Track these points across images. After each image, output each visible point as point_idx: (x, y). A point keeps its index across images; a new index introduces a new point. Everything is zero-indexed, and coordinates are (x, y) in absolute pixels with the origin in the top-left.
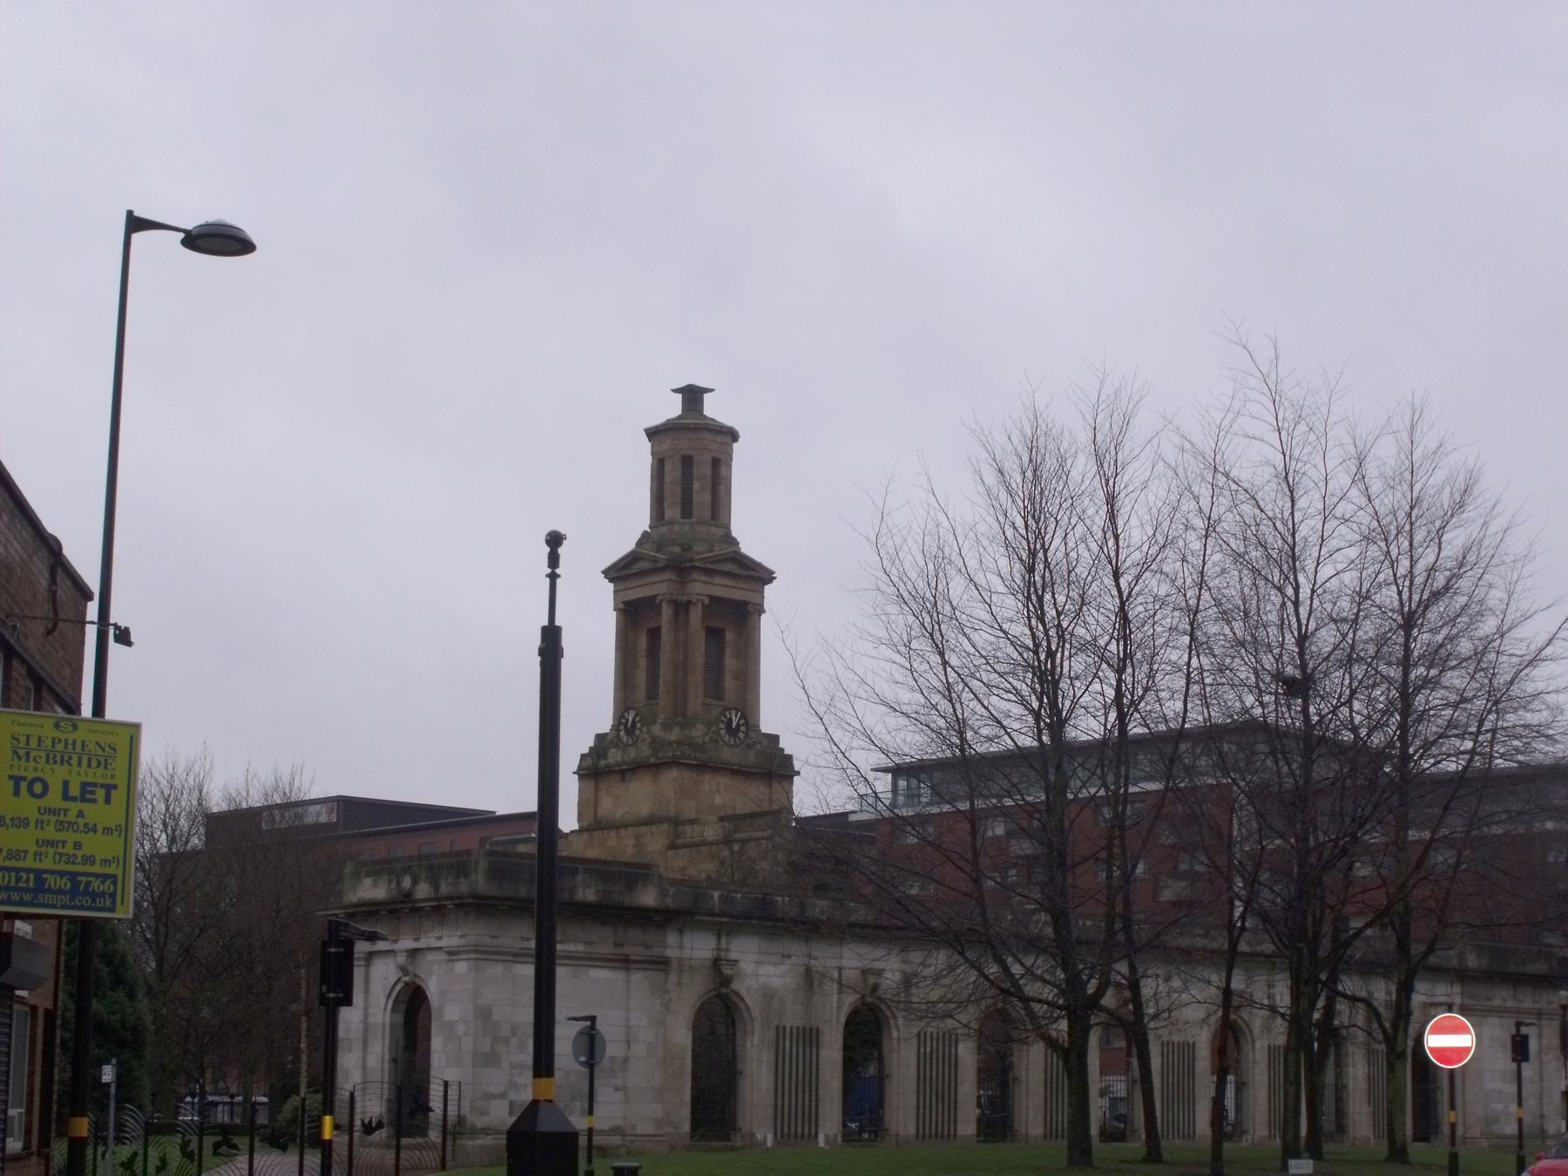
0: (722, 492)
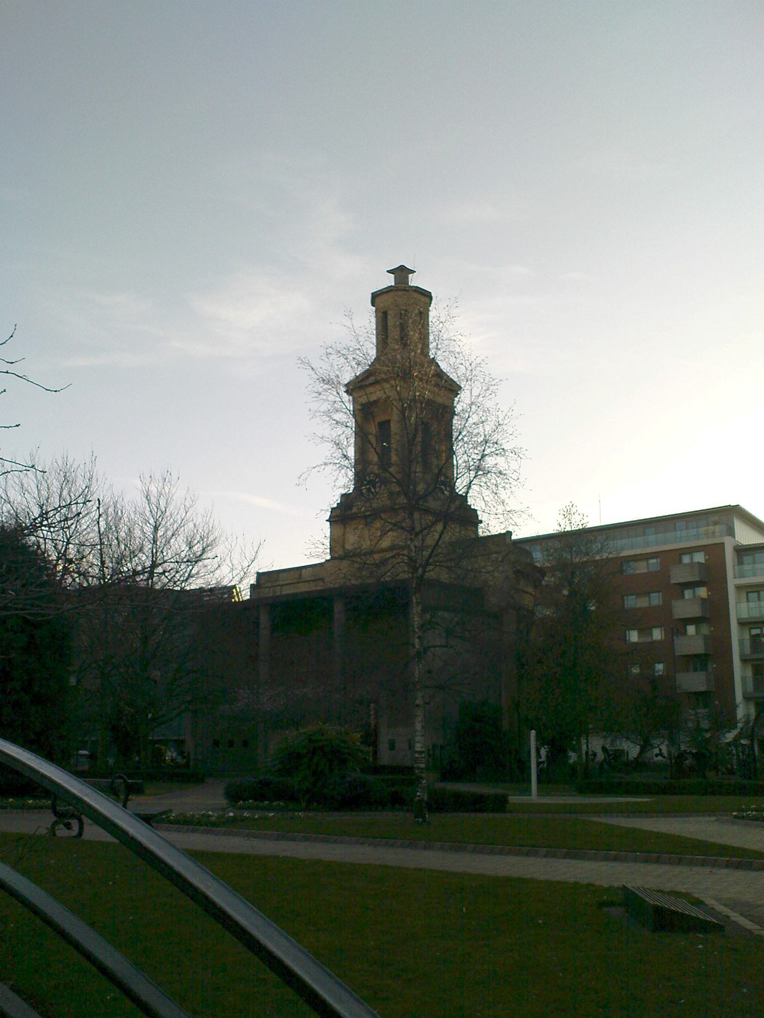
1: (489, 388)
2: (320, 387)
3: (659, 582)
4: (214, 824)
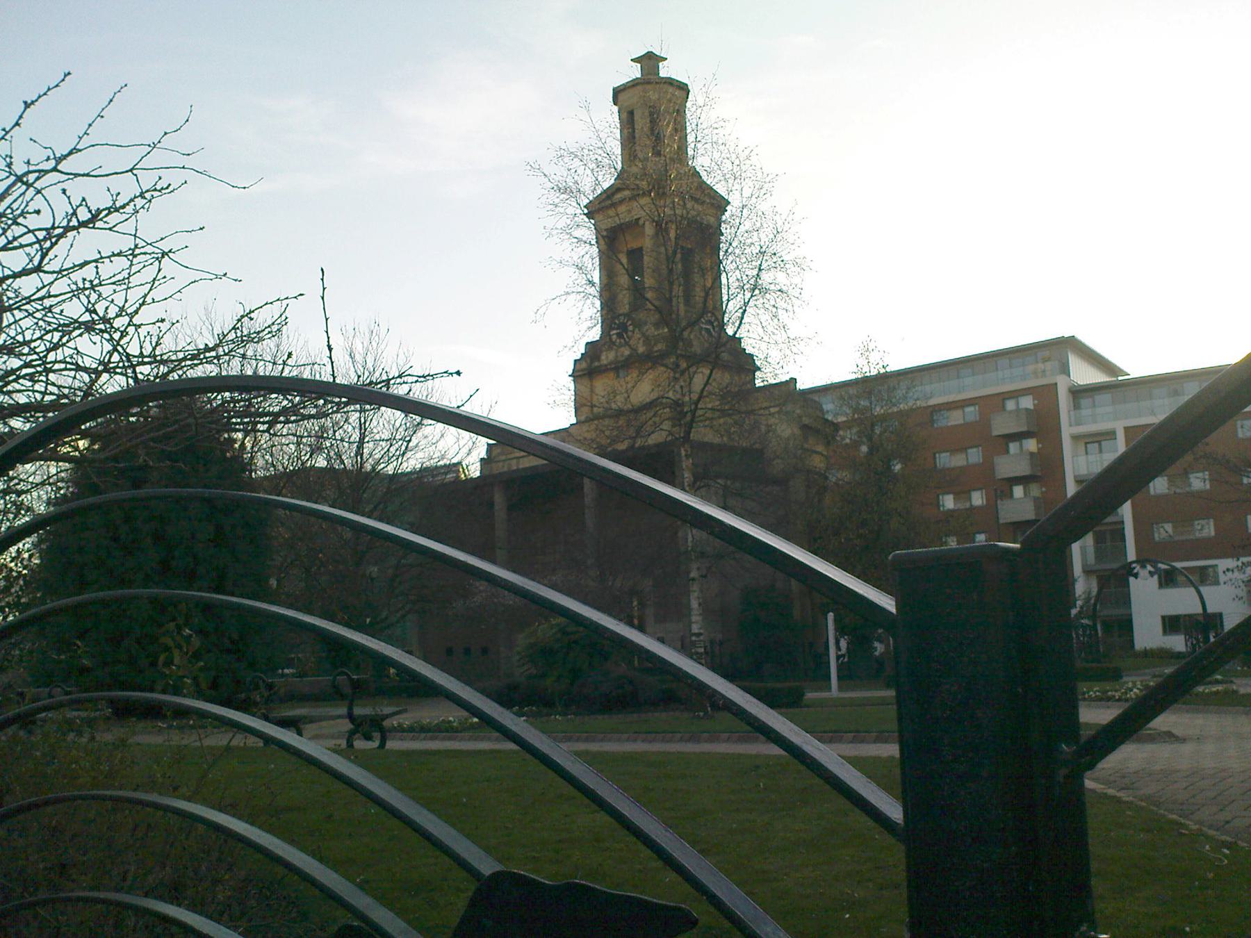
1: (762, 190)
2: (555, 197)
3: (978, 434)
4: (456, 730)
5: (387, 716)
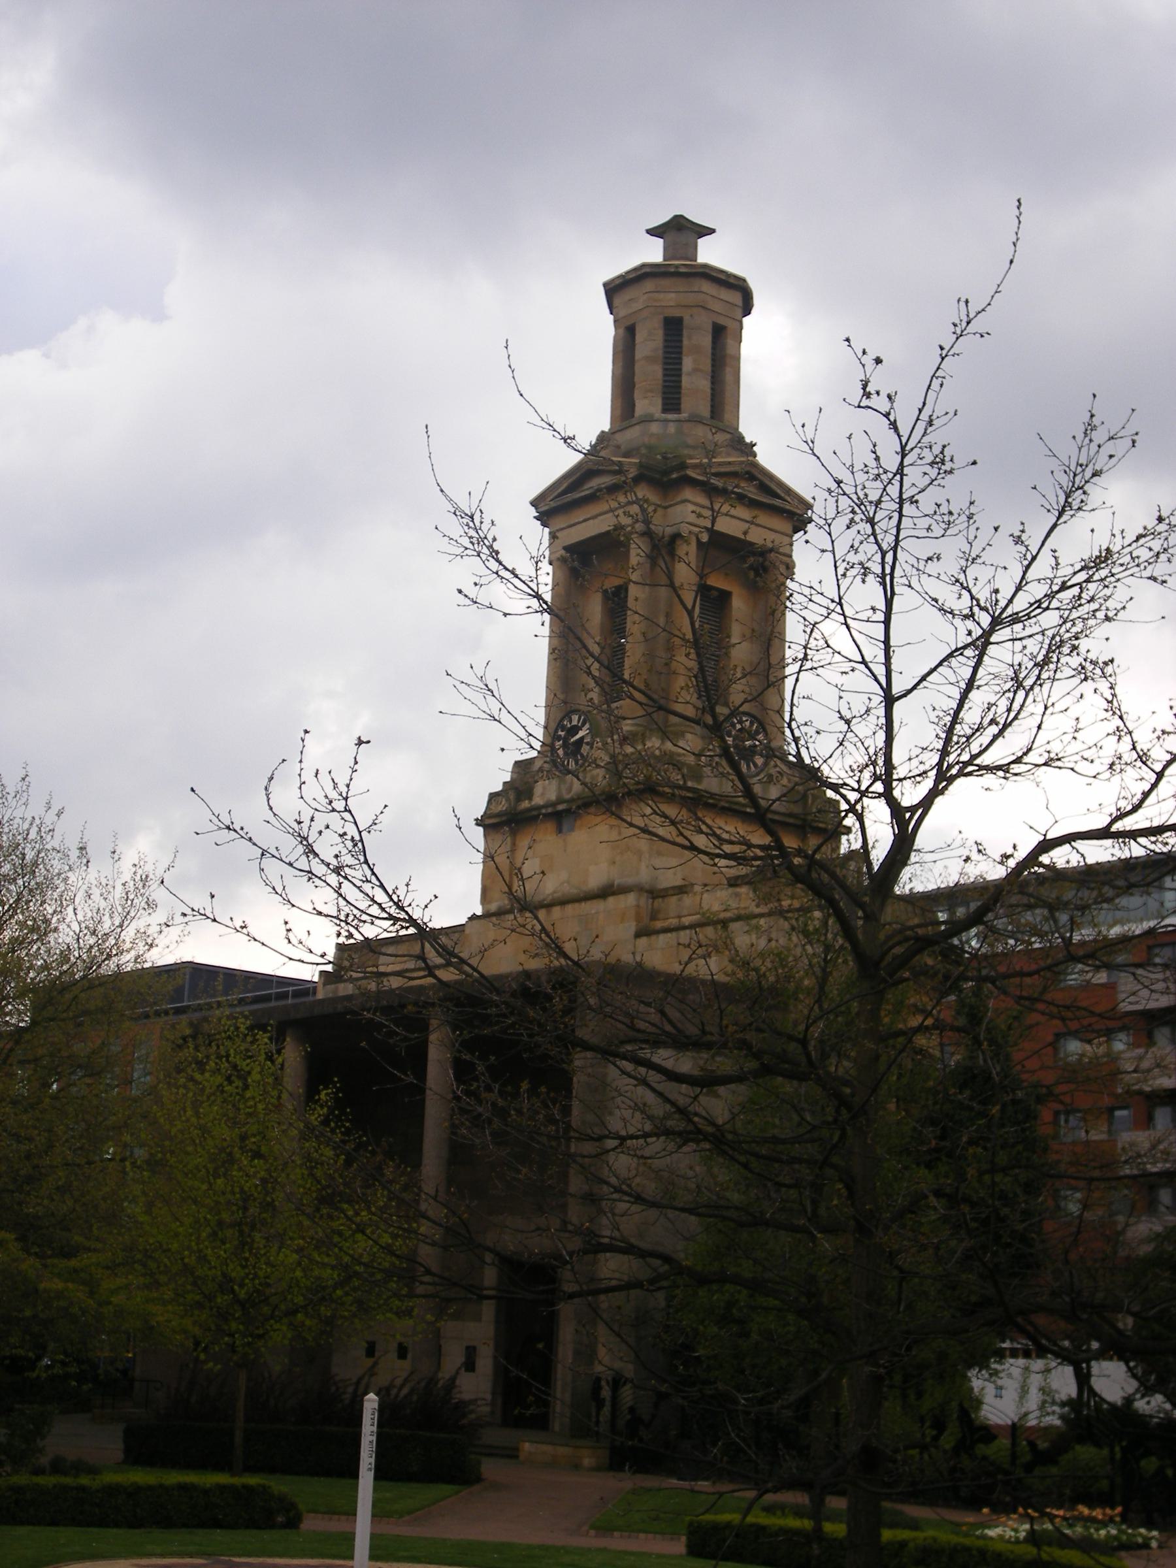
0: (729, 378)
5: (623, 1023)
